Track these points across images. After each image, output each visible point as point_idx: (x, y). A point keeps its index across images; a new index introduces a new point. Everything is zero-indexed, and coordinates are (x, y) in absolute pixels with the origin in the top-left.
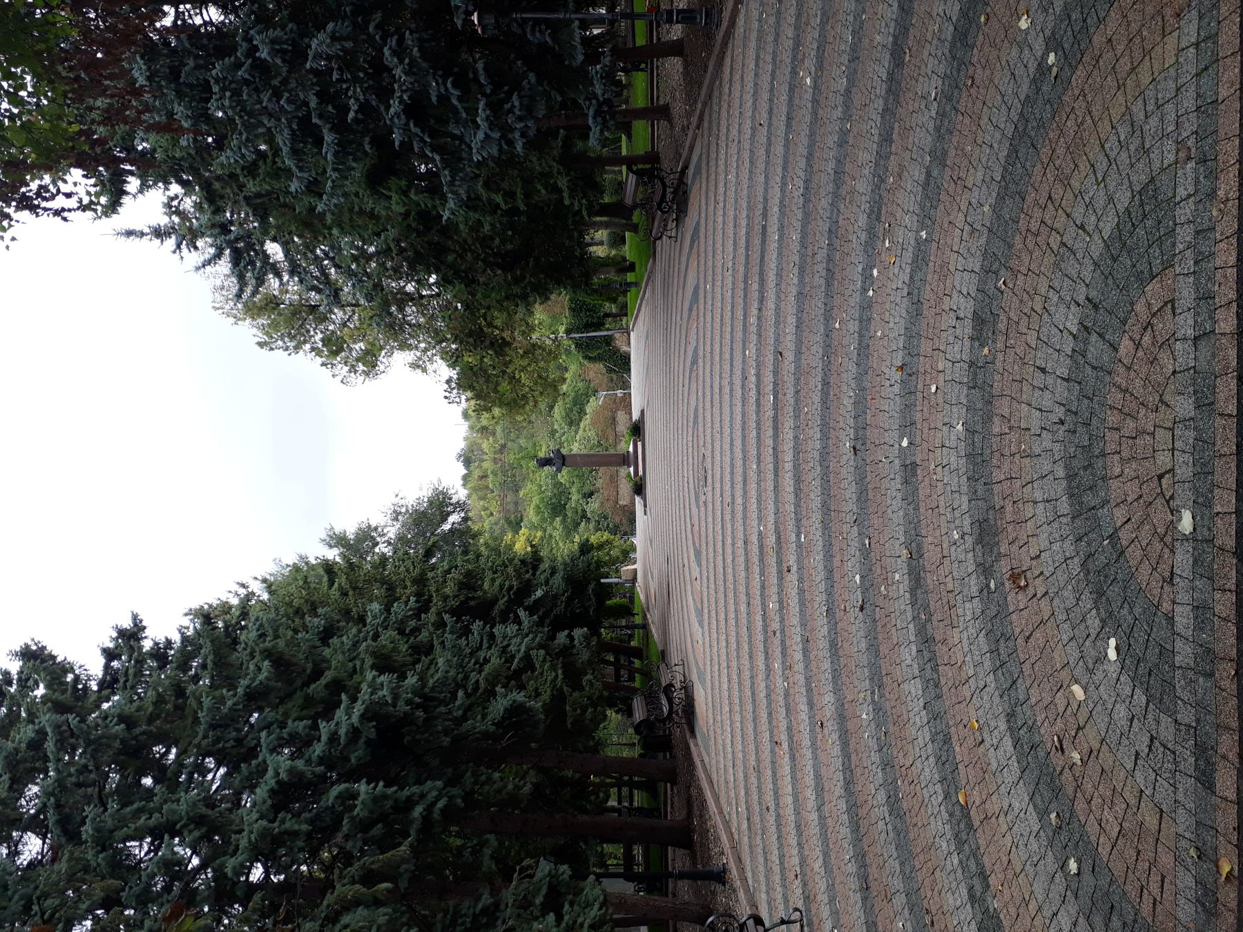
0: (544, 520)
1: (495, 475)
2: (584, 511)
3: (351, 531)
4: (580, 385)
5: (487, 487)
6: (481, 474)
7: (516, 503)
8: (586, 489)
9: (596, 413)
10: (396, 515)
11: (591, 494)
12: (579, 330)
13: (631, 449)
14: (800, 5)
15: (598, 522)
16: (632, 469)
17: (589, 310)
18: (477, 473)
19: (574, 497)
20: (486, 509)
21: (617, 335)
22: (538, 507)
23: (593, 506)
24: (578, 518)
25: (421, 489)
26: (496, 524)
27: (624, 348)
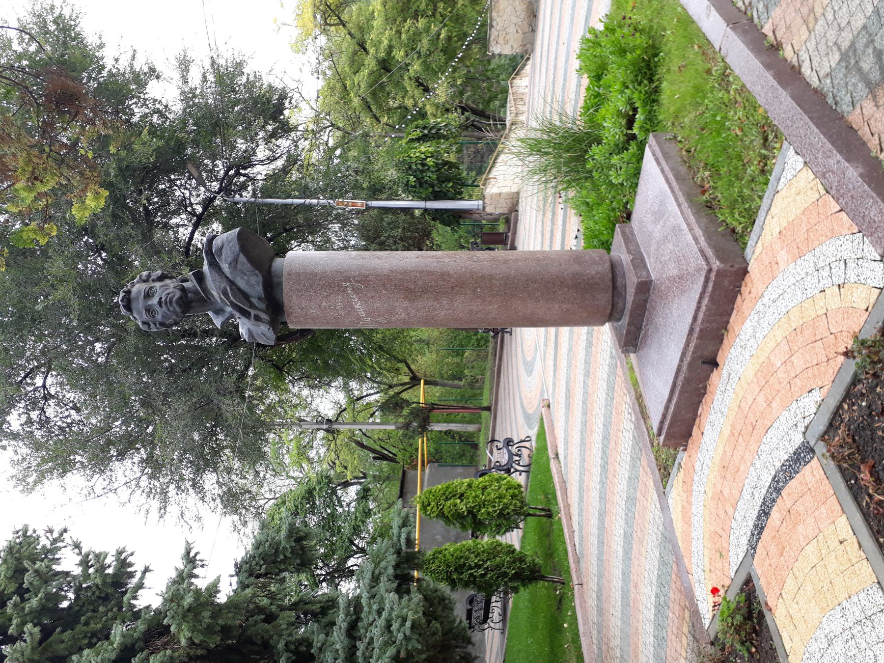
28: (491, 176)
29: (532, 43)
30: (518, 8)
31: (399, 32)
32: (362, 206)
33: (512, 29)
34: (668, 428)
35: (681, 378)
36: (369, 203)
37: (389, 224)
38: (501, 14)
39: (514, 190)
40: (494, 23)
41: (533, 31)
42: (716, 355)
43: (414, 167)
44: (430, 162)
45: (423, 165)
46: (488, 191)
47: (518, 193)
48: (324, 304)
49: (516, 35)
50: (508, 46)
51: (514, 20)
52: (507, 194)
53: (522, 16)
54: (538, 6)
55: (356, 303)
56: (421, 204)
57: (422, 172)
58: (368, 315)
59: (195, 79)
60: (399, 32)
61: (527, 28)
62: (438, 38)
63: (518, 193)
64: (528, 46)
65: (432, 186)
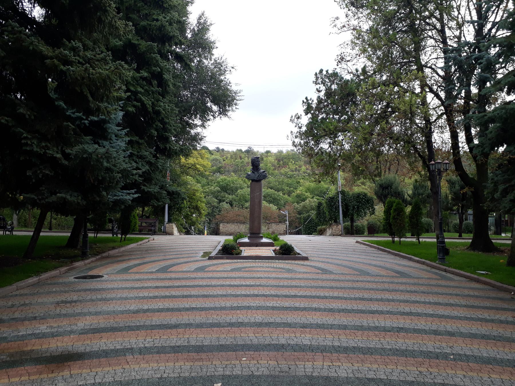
0: (218, 182)
1: (242, 163)
2: (224, 201)
3: (212, 35)
4: (282, 202)
5: (236, 159)
6: (242, 157)
7: (228, 171)
8: (235, 203)
9: (270, 209)
10: (218, 65)
11: (231, 205)
12: (343, 200)
13: (264, 240)
14: (511, 340)
15: (217, 208)
16: (246, 240)
17: (358, 208)
18: (243, 156)
19: (230, 197)
20: (226, 158)
21: (340, 227)
22: (225, 180)
23: (225, 205)
24: (219, 198)
25: (236, 84)
26: (220, 162)
27: (329, 231)
33: (227, 229)
41: (226, 235)
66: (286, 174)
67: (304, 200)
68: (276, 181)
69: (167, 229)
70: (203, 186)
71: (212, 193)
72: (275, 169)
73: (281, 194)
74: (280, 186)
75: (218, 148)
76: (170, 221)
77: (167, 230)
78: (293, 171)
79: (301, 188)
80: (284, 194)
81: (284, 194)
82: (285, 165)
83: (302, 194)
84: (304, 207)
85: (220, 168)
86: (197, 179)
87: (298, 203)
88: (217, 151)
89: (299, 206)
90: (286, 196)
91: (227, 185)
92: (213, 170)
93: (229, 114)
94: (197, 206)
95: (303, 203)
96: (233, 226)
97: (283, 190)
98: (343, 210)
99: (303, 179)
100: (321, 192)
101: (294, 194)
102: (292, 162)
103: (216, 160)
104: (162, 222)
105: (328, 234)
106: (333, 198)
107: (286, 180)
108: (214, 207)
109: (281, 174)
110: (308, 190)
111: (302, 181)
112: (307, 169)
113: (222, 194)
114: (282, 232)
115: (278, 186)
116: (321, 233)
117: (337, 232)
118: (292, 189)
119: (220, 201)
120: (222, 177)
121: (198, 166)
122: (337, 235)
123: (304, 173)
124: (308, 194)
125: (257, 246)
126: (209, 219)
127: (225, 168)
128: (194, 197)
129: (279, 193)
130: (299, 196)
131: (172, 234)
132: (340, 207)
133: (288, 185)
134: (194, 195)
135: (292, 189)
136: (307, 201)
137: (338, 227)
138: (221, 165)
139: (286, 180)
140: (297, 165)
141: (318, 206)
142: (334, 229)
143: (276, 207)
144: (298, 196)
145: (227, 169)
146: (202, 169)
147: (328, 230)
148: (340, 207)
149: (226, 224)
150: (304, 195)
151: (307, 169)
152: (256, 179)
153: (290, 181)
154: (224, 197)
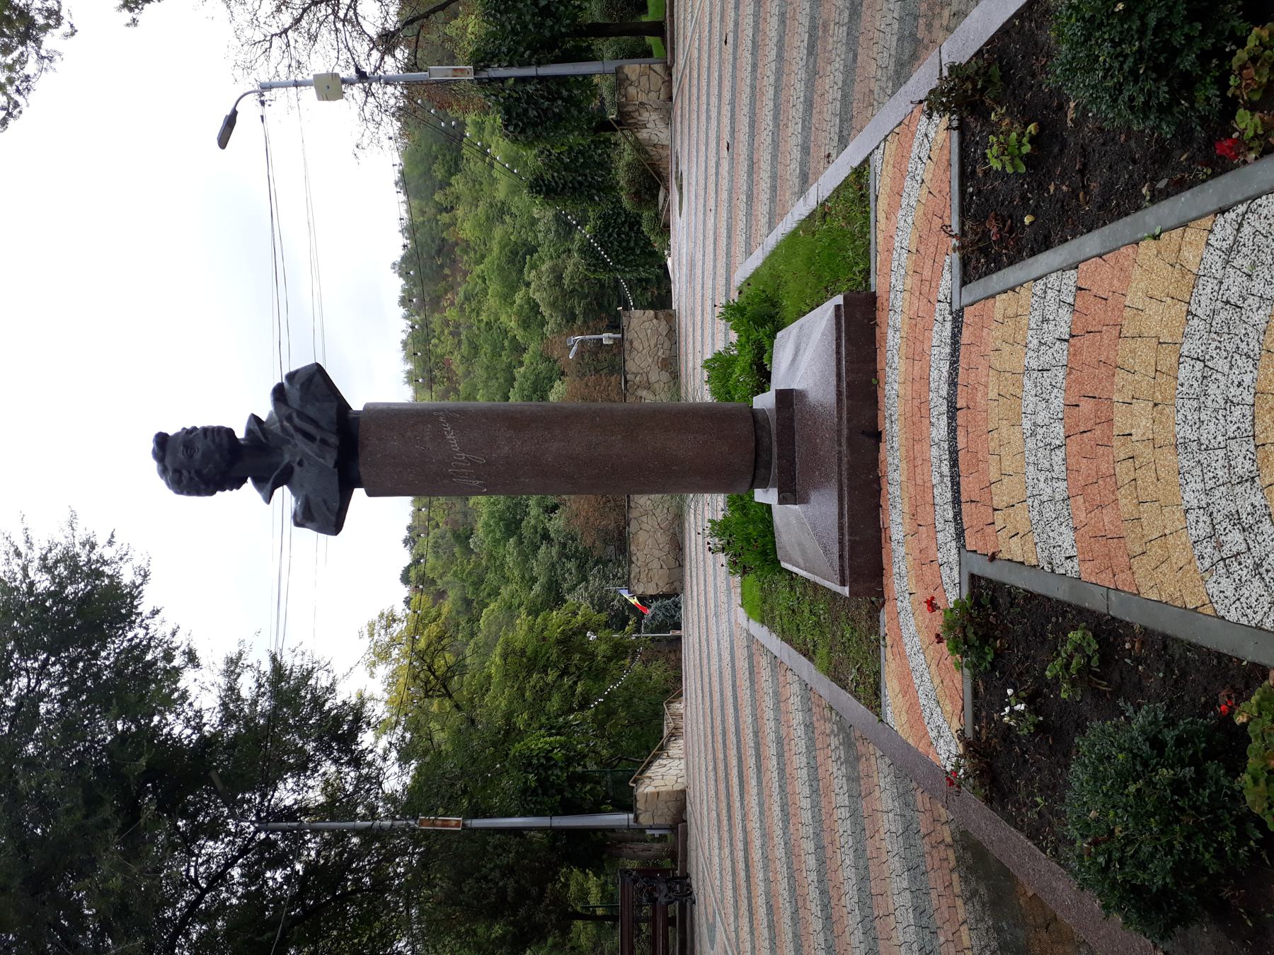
0: (496, 542)
4: (542, 367)
7: (465, 515)
15: (564, 545)
22: (487, 524)
26: (443, 537)
28: (648, 774)
29: (681, 580)
30: (661, 541)
31: (521, 690)
32: (457, 826)
33: (655, 564)
34: (850, 558)
35: (845, 467)
36: (468, 822)
37: (495, 847)
38: (641, 547)
39: (678, 787)
40: (634, 559)
41: (681, 566)
42: (877, 424)
43: (535, 761)
44: (558, 754)
45: (549, 759)
46: (640, 790)
47: (683, 792)
48: (409, 434)
49: (661, 572)
50: (653, 585)
51: (657, 553)
52: (668, 793)
53: (666, 549)
54: (683, 538)
55: (449, 433)
56: (543, 822)
57: (546, 769)
58: (462, 450)
59: (246, 686)
60: (521, 690)
61: (673, 564)
62: (573, 694)
63: (683, 792)
64: (677, 584)
65: (560, 791)
66: (467, 360)
67: (535, 307)
68: (486, 386)
69: (658, 821)
70: (507, 581)
71: (526, 560)
72: (456, 391)
73: (522, 370)
74: (502, 377)
75: (406, 542)
76: (626, 803)
77: (663, 818)
78: (460, 342)
79: (503, 318)
80: (521, 364)
81: (521, 364)
82: (444, 364)
83: (519, 314)
84: (553, 305)
85: (457, 536)
86: (489, 595)
87: (543, 323)
88: (415, 542)
89: (553, 321)
90: (526, 358)
91: (501, 519)
92: (463, 554)
93: (127, 577)
94: (558, 642)
95: (542, 309)
96: (642, 536)
97: (510, 368)
98: (557, 61)
99: (478, 314)
100: (511, 261)
101: (520, 334)
102: (436, 346)
103: (436, 546)
104: (638, 833)
105: (662, 136)
106: (508, 111)
107: (483, 359)
108: (562, 555)
109: (468, 373)
110: (507, 298)
111: (484, 317)
112: (452, 304)
113: (526, 531)
114: (663, 327)
115: (502, 380)
116: (653, 179)
117: (656, 81)
118: (506, 343)
119: (546, 536)
120: (480, 531)
121: (422, 644)
122: (669, 82)
123: (462, 310)
124: (519, 298)
125: (877, 436)
126: (596, 564)
127: (456, 522)
128: (529, 651)
129: (517, 375)
130: (524, 322)
131: (680, 800)
132: (545, 71)
133: (496, 354)
134: (523, 652)
135: (506, 343)
136: (537, 296)
137: (633, 77)
138: (449, 535)
139: (483, 359)
140: (442, 332)
141: (547, 195)
142: (642, 98)
143: (557, 383)
144: (525, 324)
145: (459, 517)
146: (433, 629)
147: (643, 135)
148: (545, 71)
149: (635, 570)
150: (521, 306)
151: (452, 304)
152: (330, 460)
153: (487, 348)
154: (535, 528)
